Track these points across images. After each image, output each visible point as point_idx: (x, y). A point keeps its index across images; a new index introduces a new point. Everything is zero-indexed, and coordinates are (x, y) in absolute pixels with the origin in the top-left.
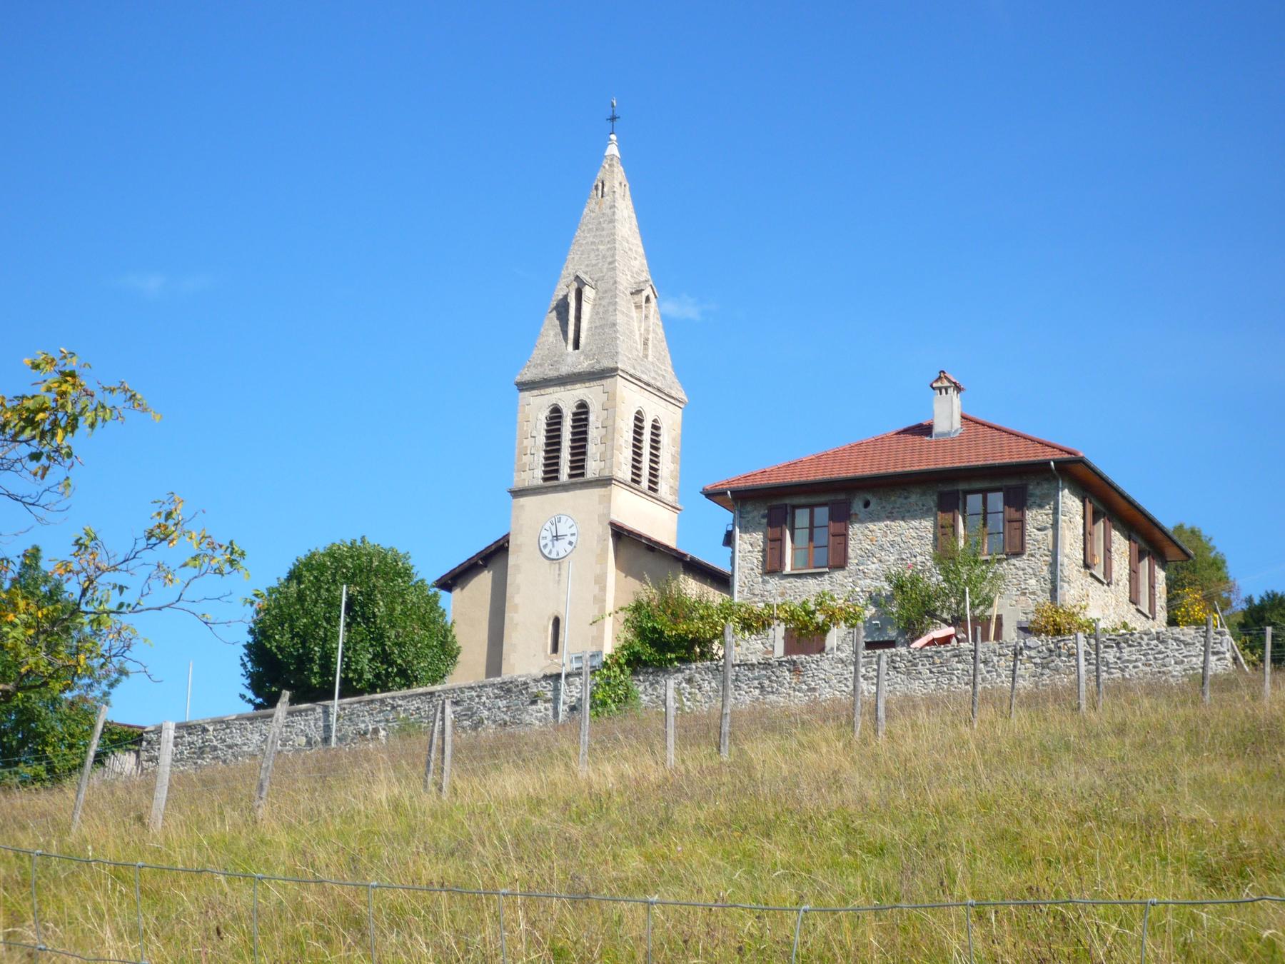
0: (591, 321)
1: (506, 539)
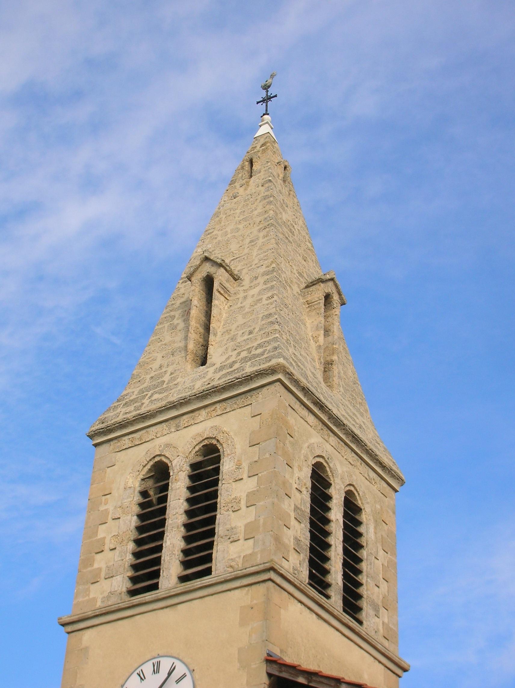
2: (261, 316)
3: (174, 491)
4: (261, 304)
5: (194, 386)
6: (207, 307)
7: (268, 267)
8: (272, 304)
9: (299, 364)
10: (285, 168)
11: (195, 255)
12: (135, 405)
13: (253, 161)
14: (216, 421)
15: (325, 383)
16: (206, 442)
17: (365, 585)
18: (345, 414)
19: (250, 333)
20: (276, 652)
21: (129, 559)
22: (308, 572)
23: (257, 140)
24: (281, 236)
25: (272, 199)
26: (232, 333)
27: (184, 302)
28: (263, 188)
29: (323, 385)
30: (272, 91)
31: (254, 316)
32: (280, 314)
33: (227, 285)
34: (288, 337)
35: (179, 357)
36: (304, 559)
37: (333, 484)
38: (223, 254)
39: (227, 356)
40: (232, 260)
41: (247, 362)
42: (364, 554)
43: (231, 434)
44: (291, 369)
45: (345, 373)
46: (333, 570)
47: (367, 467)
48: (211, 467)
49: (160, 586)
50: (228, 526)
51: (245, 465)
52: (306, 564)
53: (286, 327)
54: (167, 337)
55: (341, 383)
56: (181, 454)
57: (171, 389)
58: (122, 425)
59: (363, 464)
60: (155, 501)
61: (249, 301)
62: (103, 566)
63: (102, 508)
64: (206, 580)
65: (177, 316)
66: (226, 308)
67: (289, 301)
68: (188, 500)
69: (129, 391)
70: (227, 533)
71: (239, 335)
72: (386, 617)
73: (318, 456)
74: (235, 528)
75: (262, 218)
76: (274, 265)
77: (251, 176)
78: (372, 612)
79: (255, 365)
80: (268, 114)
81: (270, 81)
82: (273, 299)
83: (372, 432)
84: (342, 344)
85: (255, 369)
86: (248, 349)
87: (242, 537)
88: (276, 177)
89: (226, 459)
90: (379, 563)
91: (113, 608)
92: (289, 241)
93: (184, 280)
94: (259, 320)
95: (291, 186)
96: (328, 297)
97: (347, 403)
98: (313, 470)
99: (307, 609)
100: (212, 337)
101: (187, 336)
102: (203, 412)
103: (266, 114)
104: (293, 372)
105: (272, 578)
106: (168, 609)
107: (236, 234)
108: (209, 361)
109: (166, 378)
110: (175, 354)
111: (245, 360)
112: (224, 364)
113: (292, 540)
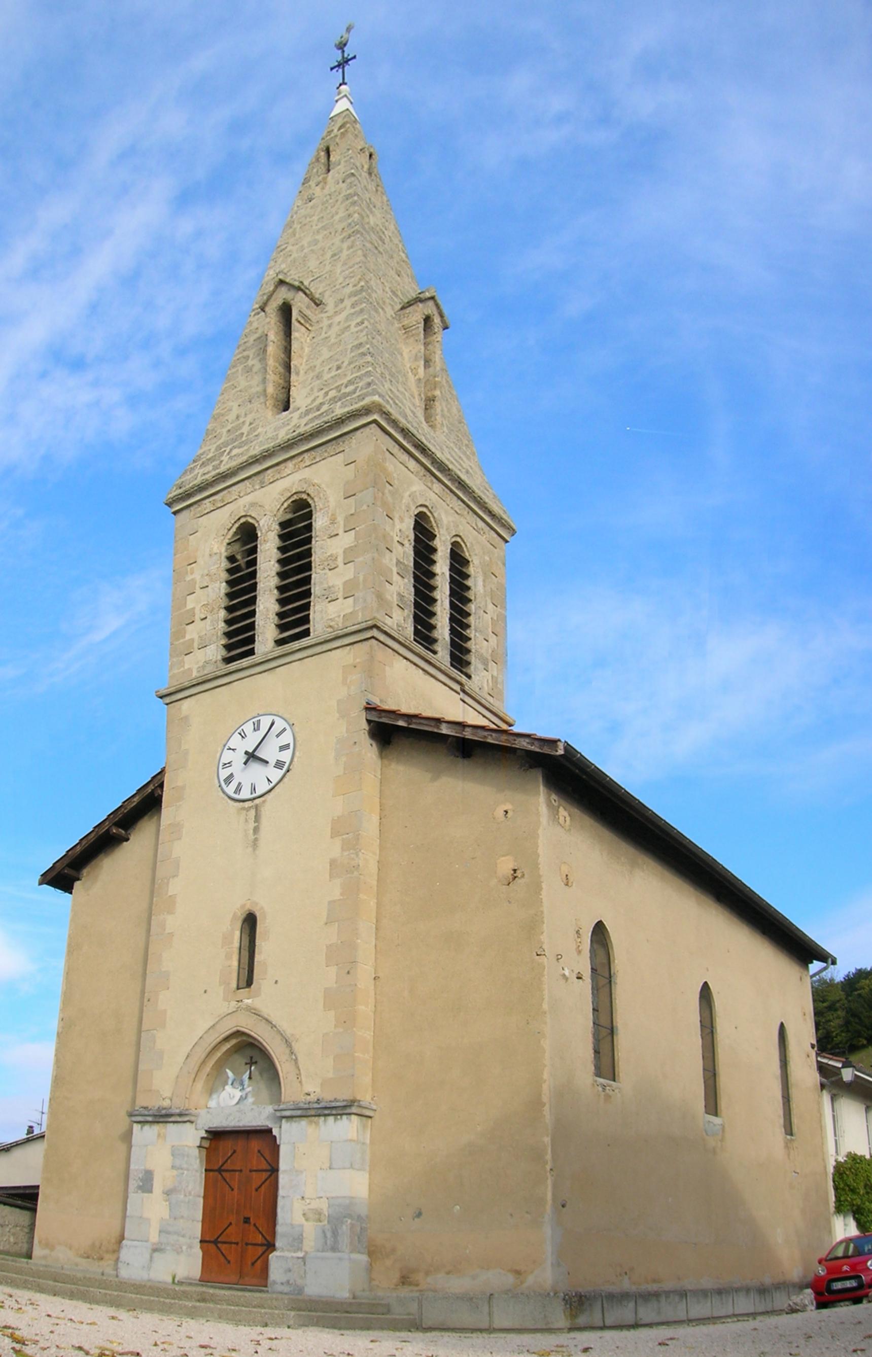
0: (356, 113)
1: (158, 781)
2: (350, 346)
3: (263, 554)
4: (349, 333)
5: (277, 435)
6: (286, 342)
7: (355, 286)
8: (362, 331)
9: (397, 402)
10: (371, 156)
11: (266, 279)
12: (213, 464)
13: (331, 149)
14: (306, 473)
15: (427, 422)
16: (295, 497)
17: (473, 639)
18: (451, 459)
19: (338, 368)
20: (376, 701)
21: (222, 626)
22: (413, 628)
23: (333, 121)
24: (368, 245)
25: (356, 198)
26: (317, 370)
27: (259, 338)
28: (344, 184)
29: (424, 425)
30: (349, 51)
31: (341, 348)
32: (372, 343)
33: (308, 312)
34: (383, 371)
35: (256, 405)
36: (408, 616)
37: (438, 536)
38: (300, 275)
39: (312, 397)
40: (312, 281)
41: (336, 402)
42: (472, 607)
43: (323, 486)
44: (388, 407)
45: (449, 410)
46: (439, 625)
47: (475, 516)
48: (303, 524)
49: (256, 651)
50: (326, 586)
51: (340, 520)
52: (411, 620)
53: (380, 358)
54: (242, 382)
55: (444, 422)
56: (268, 513)
57: (252, 442)
58: (201, 488)
59: (471, 512)
60: (243, 566)
61: (335, 329)
62: (195, 636)
63: (188, 578)
64: (304, 642)
65: (251, 356)
66: (308, 341)
67: (382, 327)
68: (279, 561)
69: (205, 449)
70: (324, 592)
71: (325, 372)
72: (495, 669)
73: (421, 506)
74: (333, 586)
75: (344, 224)
76: (362, 283)
77: (329, 171)
78: (481, 666)
79: (346, 406)
80: (346, 84)
81: (346, 36)
82: (364, 325)
83: (480, 478)
84: (444, 377)
85: (346, 409)
86: (337, 387)
87: (340, 595)
88: (359, 168)
89: (318, 514)
90: (487, 617)
91: (210, 677)
92: (379, 252)
93: (256, 311)
94: (348, 352)
95: (378, 180)
96: (427, 320)
97: (452, 445)
98: (416, 521)
99: (413, 665)
100: (293, 377)
101: (265, 378)
102: (290, 464)
103: (344, 83)
104: (391, 410)
105: (375, 635)
106: (266, 673)
107: (314, 248)
108: (292, 406)
109: (245, 429)
110: (253, 401)
111: (334, 400)
112: (310, 407)
113: (395, 596)
